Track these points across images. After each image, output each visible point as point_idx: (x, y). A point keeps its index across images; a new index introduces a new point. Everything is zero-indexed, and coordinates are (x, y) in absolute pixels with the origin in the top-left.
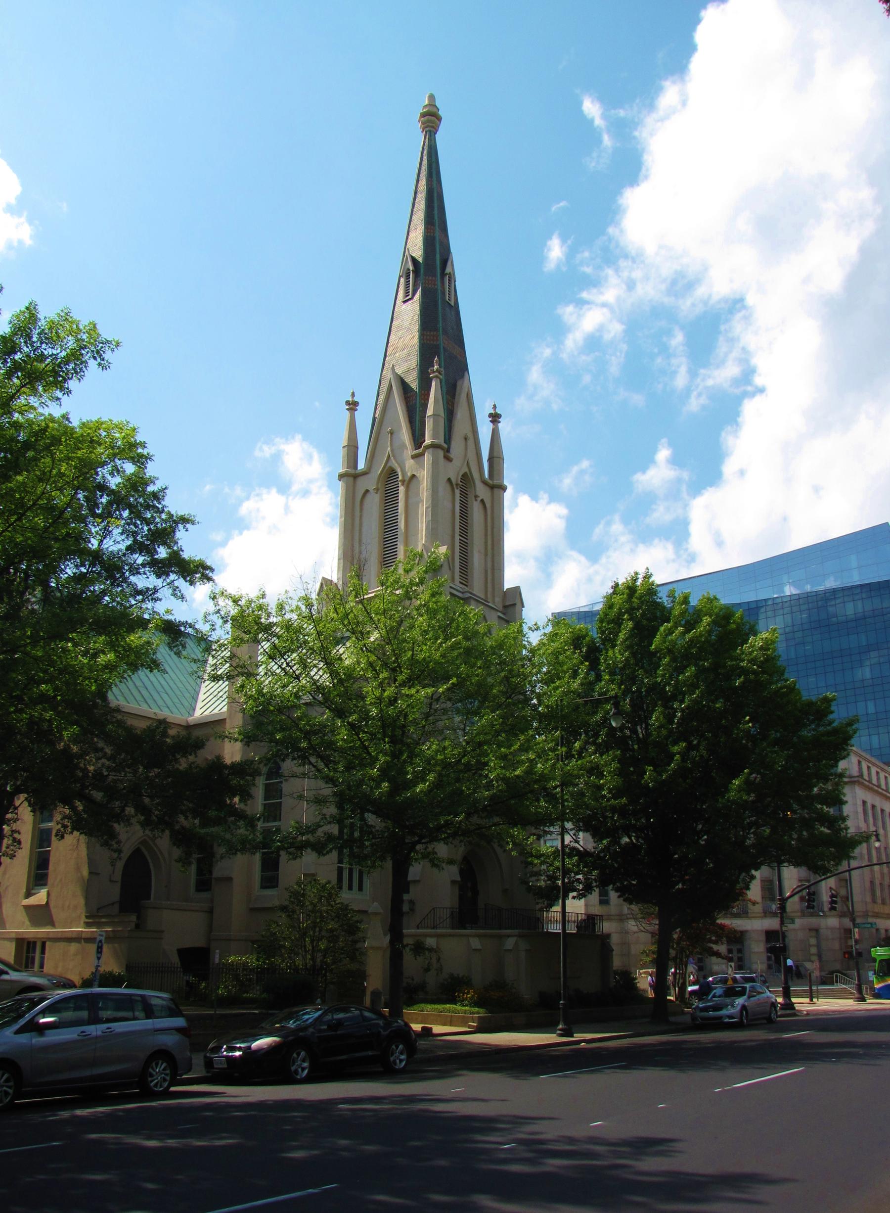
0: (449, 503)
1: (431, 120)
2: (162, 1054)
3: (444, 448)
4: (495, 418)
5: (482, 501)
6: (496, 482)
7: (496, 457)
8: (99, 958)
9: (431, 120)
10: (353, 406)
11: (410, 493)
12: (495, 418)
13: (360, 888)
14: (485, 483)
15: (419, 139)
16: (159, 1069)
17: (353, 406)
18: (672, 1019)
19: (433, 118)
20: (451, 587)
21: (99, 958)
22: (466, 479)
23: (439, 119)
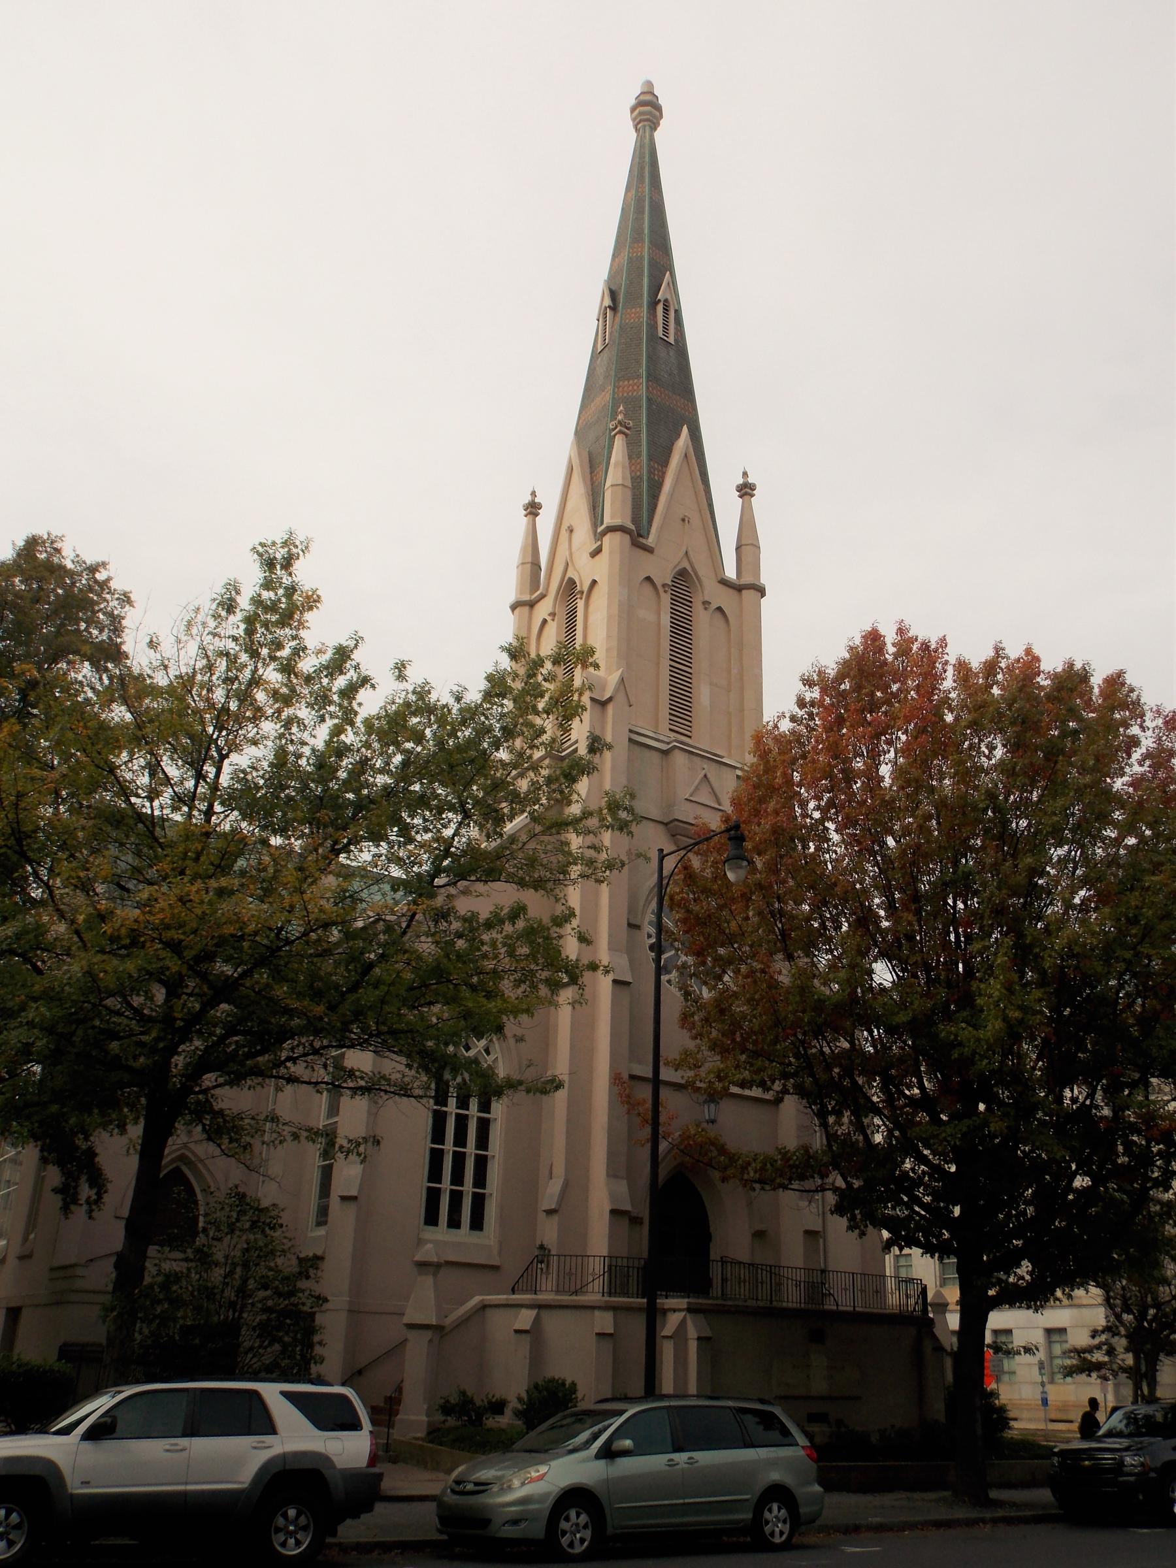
0: (658, 616)
1: (648, 112)
2: (778, 1493)
3: (636, 536)
4: (746, 490)
5: (719, 609)
6: (747, 579)
7: (747, 544)
8: (1044, 1392)
9: (648, 112)
10: (533, 509)
11: (591, 608)
12: (746, 490)
13: (477, 1223)
14: (725, 582)
15: (629, 137)
16: (775, 1513)
17: (533, 509)
18: (994, 1494)
19: (648, 108)
20: (631, 731)
21: (1044, 1392)
22: (683, 580)
23: (659, 108)
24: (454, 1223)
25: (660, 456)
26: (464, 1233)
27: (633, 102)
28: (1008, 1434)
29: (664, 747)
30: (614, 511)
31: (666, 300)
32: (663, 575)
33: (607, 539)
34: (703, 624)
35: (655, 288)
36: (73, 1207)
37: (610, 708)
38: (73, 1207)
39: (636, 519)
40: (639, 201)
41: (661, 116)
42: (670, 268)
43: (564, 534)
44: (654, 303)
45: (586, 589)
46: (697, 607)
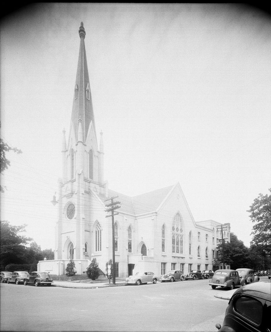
10: (64, 132)
17: (64, 132)
23: (85, 32)
24: (99, 250)
25: (87, 128)
26: (100, 251)
27: (80, 37)
28: (268, 306)
29: (89, 182)
30: (80, 139)
31: (88, 90)
32: (88, 150)
33: (79, 143)
34: (95, 160)
35: (86, 87)
36: (26, 224)
37: (81, 175)
38: (26, 224)
39: (83, 140)
40: (82, 70)
41: (85, 35)
42: (89, 82)
43: (71, 140)
44: (86, 90)
45: (75, 151)
46: (93, 156)
